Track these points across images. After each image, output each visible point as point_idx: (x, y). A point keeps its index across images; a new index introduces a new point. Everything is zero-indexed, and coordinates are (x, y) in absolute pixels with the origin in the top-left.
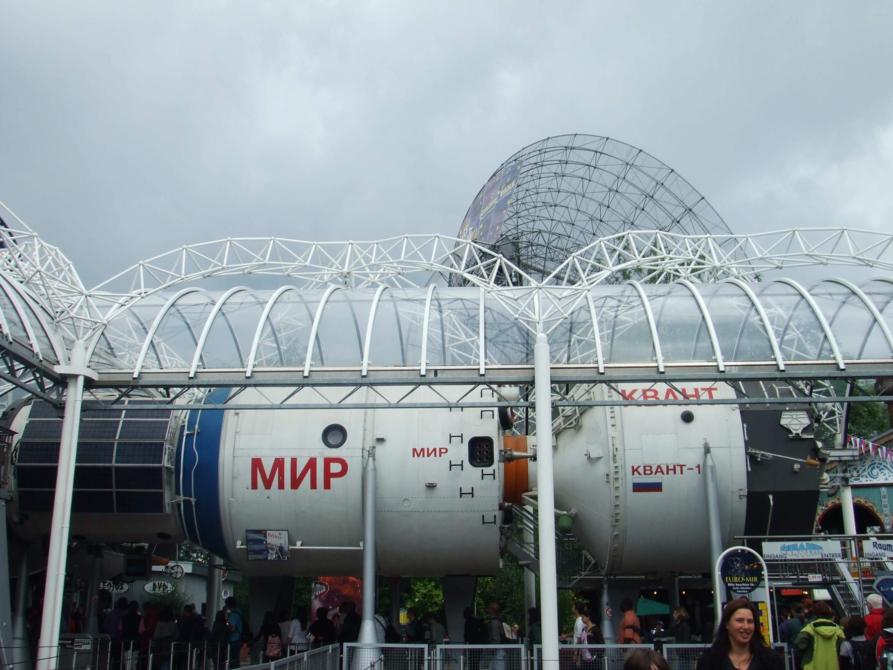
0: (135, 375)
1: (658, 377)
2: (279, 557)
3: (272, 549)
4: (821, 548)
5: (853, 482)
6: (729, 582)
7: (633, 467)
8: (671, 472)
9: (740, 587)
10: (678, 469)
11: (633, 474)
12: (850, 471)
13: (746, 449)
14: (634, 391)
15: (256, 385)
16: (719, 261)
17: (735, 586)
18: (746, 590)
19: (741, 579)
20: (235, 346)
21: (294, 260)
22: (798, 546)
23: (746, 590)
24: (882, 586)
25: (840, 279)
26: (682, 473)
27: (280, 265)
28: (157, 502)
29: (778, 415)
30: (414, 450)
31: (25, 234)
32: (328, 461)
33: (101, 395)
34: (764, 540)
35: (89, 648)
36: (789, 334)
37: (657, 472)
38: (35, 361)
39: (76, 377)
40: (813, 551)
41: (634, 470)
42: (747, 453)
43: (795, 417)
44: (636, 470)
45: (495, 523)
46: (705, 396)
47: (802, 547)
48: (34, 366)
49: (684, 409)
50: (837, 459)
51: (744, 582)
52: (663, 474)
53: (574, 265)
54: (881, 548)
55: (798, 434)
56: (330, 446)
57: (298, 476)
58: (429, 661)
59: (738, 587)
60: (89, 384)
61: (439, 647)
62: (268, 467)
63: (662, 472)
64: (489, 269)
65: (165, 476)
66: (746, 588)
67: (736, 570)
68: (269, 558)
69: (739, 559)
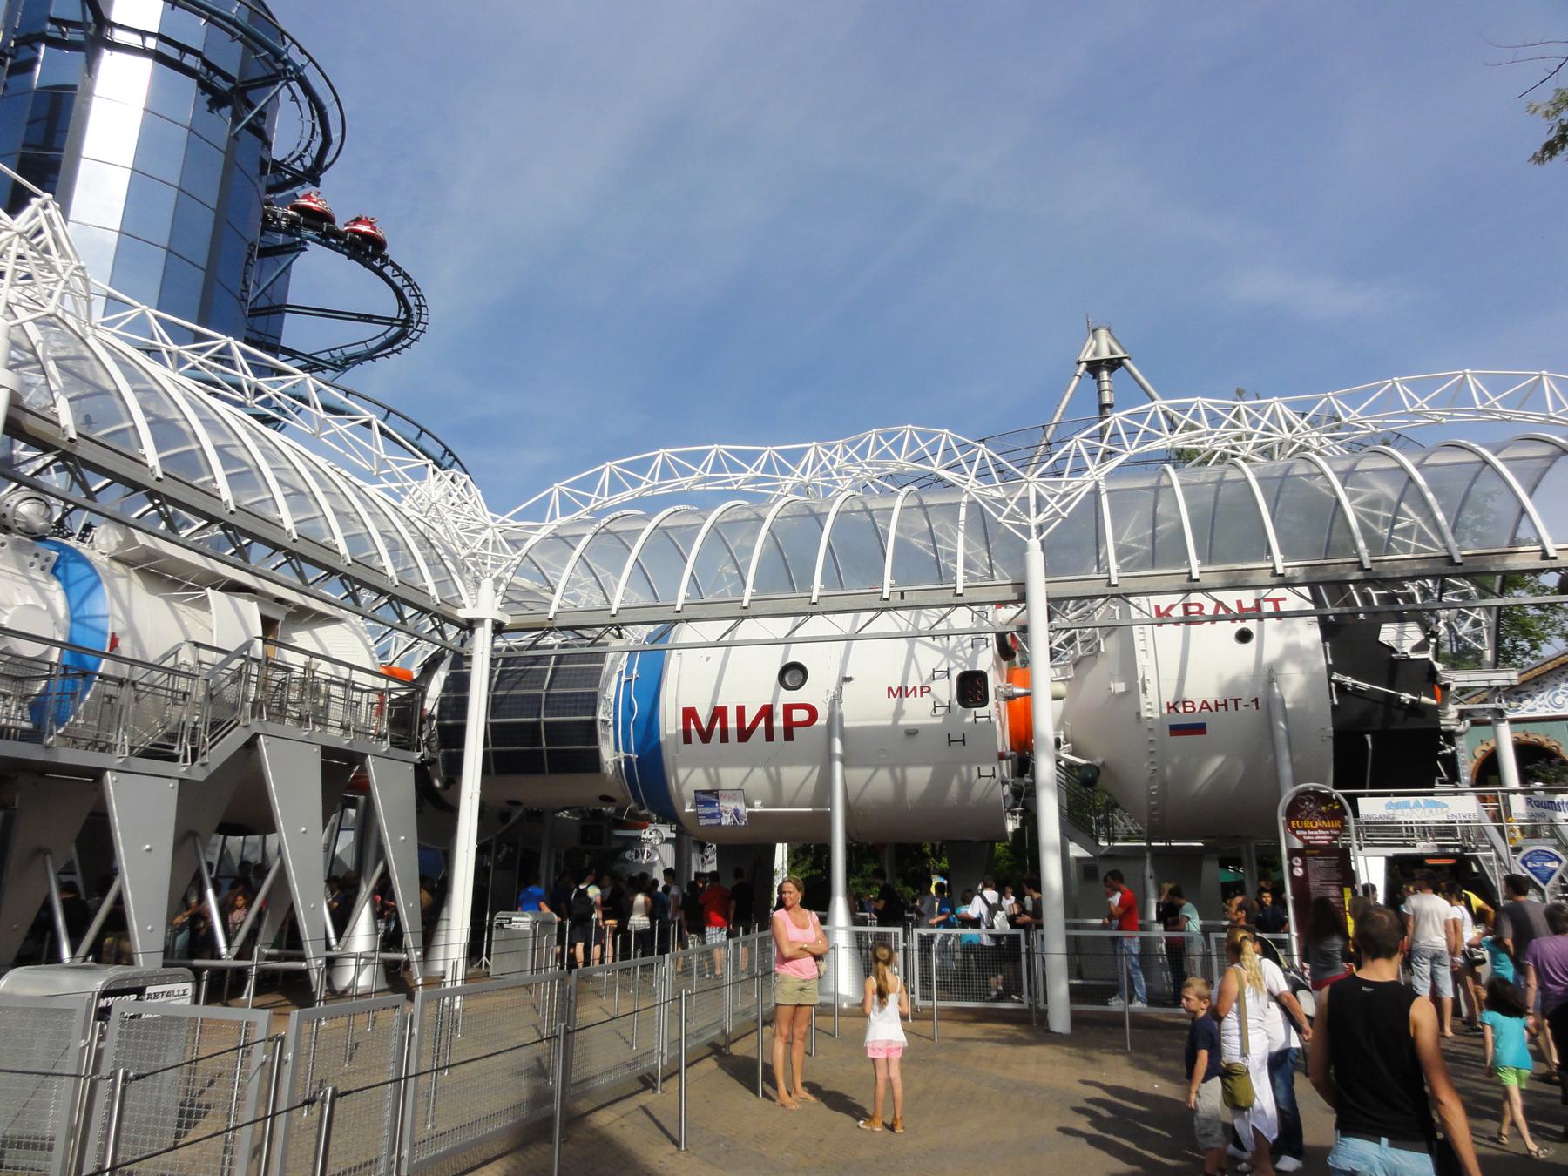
0: (551, 616)
1: (1190, 585)
2: (734, 822)
3: (726, 812)
4: (1446, 806)
5: (1510, 715)
6: (1298, 829)
10: (1231, 704)
13: (1330, 675)
14: (1172, 607)
15: (755, 617)
16: (1290, 431)
17: (1308, 835)
20: (235, 616)
21: (745, 471)
22: (1412, 804)
24: (1530, 860)
25: (1473, 445)
26: (1237, 709)
27: (728, 478)
28: (592, 761)
30: (890, 689)
31: (1339, 405)
32: (788, 709)
33: (513, 641)
34: (1363, 795)
35: (528, 929)
36: (1400, 521)
37: (1202, 708)
38: (431, 605)
39: (481, 621)
40: (1434, 810)
45: (994, 776)
46: (1268, 607)
47: (1417, 805)
48: (431, 611)
49: (1239, 625)
50: (1486, 684)
52: (1211, 710)
53: (1078, 450)
56: (788, 688)
57: (747, 725)
58: (905, 949)
60: (499, 628)
61: (916, 931)
62: (704, 715)
63: (1209, 707)
64: (970, 462)
65: (600, 731)
68: (723, 823)
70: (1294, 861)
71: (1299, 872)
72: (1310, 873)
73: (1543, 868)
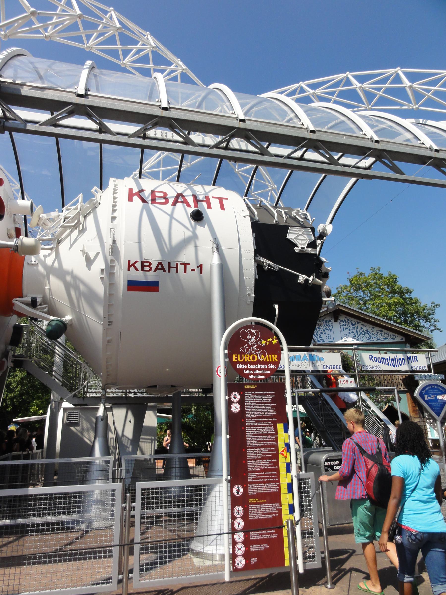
7: (129, 262)
8: (173, 270)
9: (254, 370)
11: (129, 269)
12: (326, 321)
17: (247, 369)
18: (261, 374)
19: (254, 358)
23: (261, 374)
26: (185, 272)
29: (284, 229)
37: (157, 268)
41: (130, 265)
42: (256, 261)
43: (301, 233)
44: (133, 265)
51: (259, 362)
54: (376, 361)
55: (303, 248)
59: (250, 369)
63: (163, 269)
66: (262, 372)
67: (250, 346)
69: (254, 332)
70: (232, 397)
71: (236, 408)
72: (247, 409)
73: (436, 400)
